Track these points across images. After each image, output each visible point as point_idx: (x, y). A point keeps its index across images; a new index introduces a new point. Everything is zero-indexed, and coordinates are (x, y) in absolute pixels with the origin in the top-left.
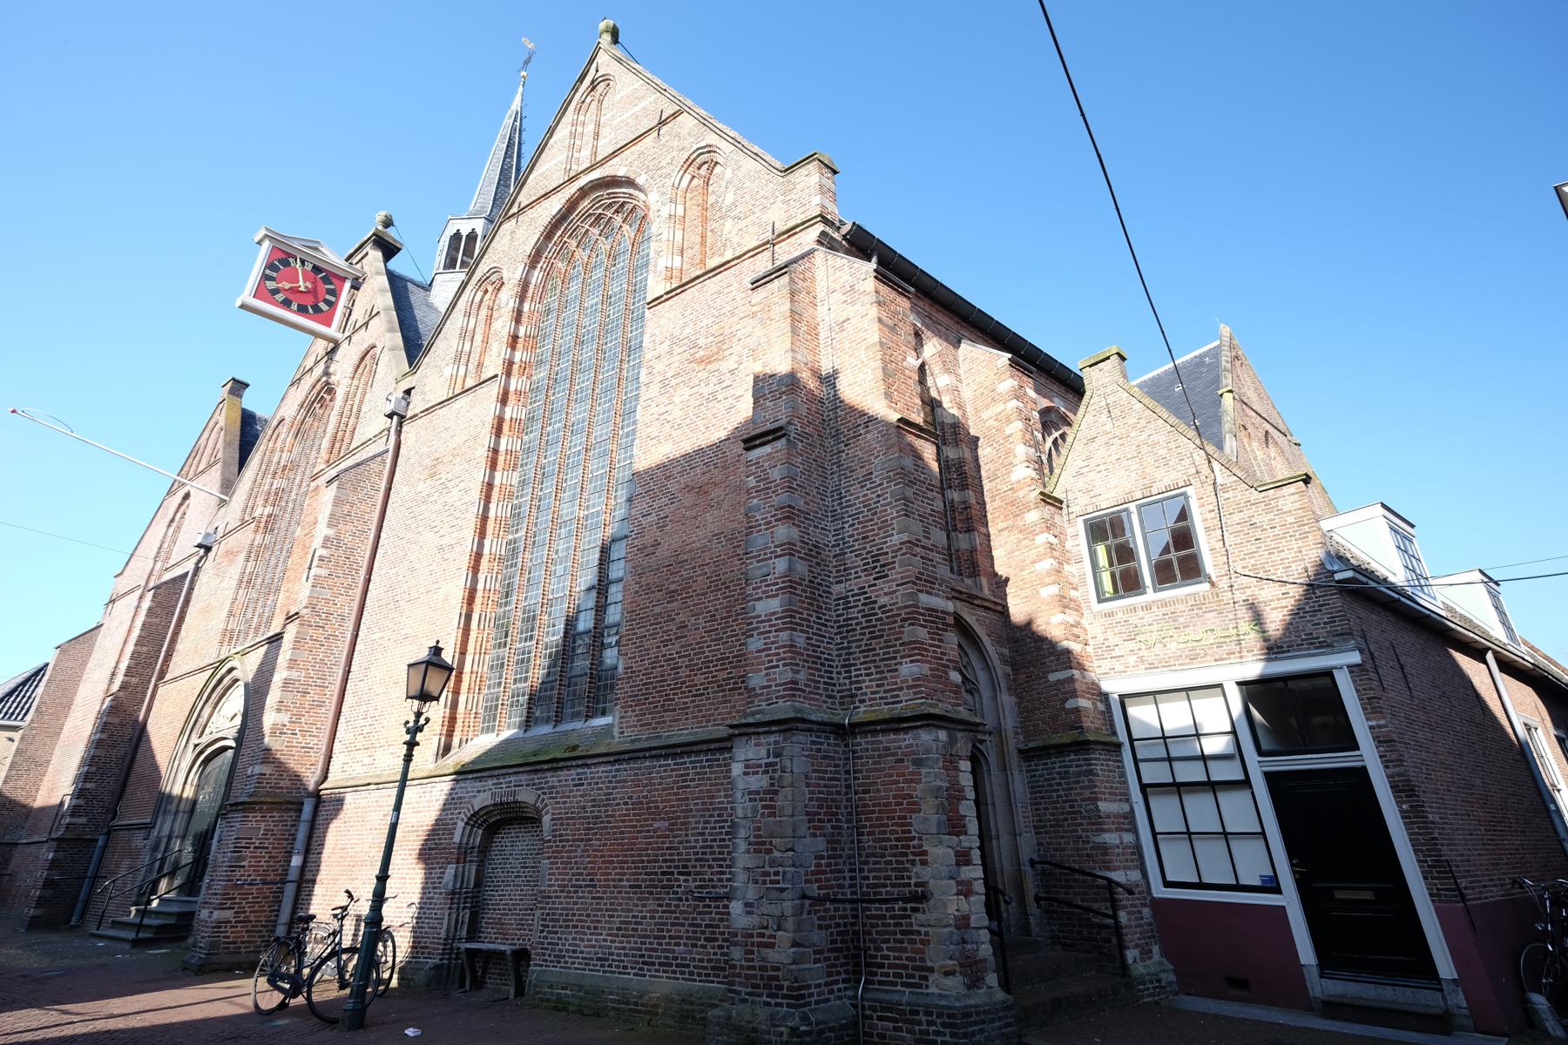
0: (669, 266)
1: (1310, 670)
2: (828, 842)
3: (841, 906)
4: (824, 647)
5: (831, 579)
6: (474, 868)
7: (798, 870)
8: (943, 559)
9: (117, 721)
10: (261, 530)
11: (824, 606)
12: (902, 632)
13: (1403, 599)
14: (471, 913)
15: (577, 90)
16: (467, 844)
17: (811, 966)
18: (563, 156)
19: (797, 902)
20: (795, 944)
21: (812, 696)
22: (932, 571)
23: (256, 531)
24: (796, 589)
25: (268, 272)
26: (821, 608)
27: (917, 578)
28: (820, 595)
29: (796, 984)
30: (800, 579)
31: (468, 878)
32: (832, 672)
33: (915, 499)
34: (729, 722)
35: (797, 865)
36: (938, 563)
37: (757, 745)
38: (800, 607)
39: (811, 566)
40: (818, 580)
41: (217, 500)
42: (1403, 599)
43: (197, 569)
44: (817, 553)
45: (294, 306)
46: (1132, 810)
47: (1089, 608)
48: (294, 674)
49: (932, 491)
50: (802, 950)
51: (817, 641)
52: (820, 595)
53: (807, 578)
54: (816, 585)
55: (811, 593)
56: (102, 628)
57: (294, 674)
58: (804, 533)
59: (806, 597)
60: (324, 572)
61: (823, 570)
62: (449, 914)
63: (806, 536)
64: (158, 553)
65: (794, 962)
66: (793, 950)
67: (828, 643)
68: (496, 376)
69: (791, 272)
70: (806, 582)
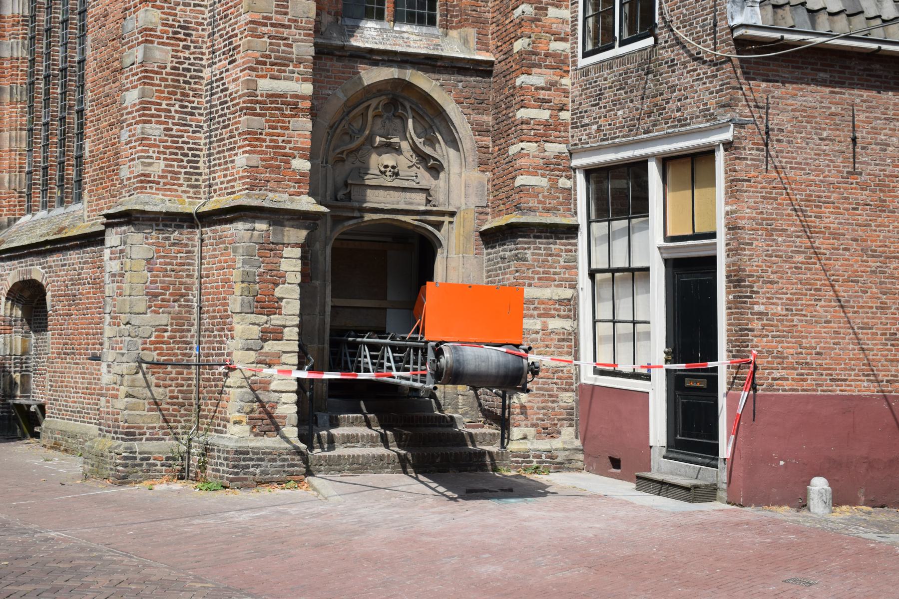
1: (676, 151)
2: (172, 318)
4: (188, 137)
5: (204, 63)
7: (135, 339)
8: (305, 35)
11: (191, 93)
12: (238, 122)
13: (885, 47)
14: (22, 376)
16: (11, 316)
17: (145, 413)
19: (132, 364)
20: (128, 395)
21: (168, 187)
22: (283, 52)
24: (152, 79)
26: (188, 96)
27: (258, 63)
29: (126, 424)
30: (159, 67)
31: (16, 345)
32: (197, 162)
34: (106, 212)
35: (132, 335)
36: (295, 41)
37: (116, 234)
38: (159, 97)
39: (177, 51)
40: (185, 66)
42: (885, 47)
44: (185, 34)
47: (574, 63)
50: (134, 400)
51: (178, 131)
52: (185, 82)
53: (169, 65)
54: (181, 72)
55: (173, 80)
58: (169, 14)
59: (166, 86)
61: (193, 53)
62: (3, 376)
63: (171, 18)
66: (126, 399)
67: (194, 132)
70: (168, 70)
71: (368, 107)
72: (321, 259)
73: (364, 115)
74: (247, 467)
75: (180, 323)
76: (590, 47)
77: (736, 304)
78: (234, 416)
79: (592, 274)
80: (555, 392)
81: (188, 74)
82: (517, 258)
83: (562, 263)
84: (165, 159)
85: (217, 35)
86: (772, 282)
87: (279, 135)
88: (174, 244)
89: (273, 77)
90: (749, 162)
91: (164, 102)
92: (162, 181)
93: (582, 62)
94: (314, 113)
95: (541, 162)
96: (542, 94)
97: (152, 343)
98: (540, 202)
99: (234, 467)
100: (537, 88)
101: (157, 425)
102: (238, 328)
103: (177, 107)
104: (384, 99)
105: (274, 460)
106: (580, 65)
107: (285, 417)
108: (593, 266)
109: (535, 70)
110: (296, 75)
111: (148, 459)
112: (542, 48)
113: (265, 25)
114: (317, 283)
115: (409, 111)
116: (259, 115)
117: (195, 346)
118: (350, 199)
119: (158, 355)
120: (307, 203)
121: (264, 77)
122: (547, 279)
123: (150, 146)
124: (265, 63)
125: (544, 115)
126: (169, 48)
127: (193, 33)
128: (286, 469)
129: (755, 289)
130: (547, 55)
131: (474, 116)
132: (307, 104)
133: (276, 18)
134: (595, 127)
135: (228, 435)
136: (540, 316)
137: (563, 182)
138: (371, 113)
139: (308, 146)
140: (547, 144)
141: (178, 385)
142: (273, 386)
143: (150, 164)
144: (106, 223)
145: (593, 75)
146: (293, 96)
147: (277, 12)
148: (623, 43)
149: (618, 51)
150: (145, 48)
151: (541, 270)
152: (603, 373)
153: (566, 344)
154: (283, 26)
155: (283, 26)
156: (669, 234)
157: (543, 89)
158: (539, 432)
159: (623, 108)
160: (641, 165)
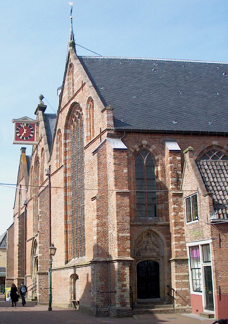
0: (87, 136)
3: (107, 293)
6: (73, 286)
9: (20, 251)
10: (34, 201)
11: (106, 236)
15: (67, 68)
18: (67, 92)
20: (96, 299)
23: (34, 201)
25: (17, 131)
28: (105, 234)
40: (105, 231)
41: (25, 191)
43: (26, 210)
45: (25, 139)
46: (189, 275)
48: (41, 245)
49: (127, 207)
52: (105, 234)
56: (15, 224)
57: (41, 245)
60: (41, 220)
64: (19, 203)
65: (96, 301)
68: (63, 165)
69: (98, 151)
71: (143, 236)
72: (134, 269)
73: (142, 237)
74: (120, 313)
75: (106, 283)
77: (216, 276)
78: (117, 302)
79: (191, 270)
80: (185, 296)
81: (106, 232)
83: (185, 267)
84: (102, 250)
85: (111, 224)
86: (223, 271)
87: (124, 245)
89: (122, 233)
90: (216, 247)
91: (101, 239)
92: (101, 254)
93: (187, 224)
94: (131, 239)
95: (179, 246)
96: (179, 231)
97: (101, 288)
98: (180, 254)
99: (118, 313)
100: (177, 230)
101: (102, 305)
102: (117, 284)
103: (104, 239)
104: (146, 234)
105: (125, 312)
107: (127, 303)
108: (192, 268)
109: (177, 226)
110: (127, 232)
111: (101, 312)
112: (178, 221)
113: (120, 223)
114: (134, 274)
115: (152, 236)
117: (109, 288)
118: (140, 256)
119: (188, 141)
120: (130, 258)
121: (120, 233)
122: (182, 271)
123: (99, 248)
124: (120, 230)
126: (101, 227)
127: (106, 224)
128: (128, 313)
129: (219, 273)
131: (166, 236)
132: (129, 238)
133: (122, 221)
135: (116, 307)
136: (181, 279)
137: (184, 250)
138: (143, 237)
139: (130, 246)
140: (180, 242)
141: (106, 296)
142: (125, 296)
143: (99, 251)
145: (189, 227)
146: (126, 237)
147: (122, 220)
149: (193, 222)
150: (97, 228)
151: (180, 269)
152: (195, 291)
153: (187, 285)
154: (123, 223)
155: (123, 223)
156: (204, 261)
157: (179, 230)
158: (182, 305)
160: (198, 246)
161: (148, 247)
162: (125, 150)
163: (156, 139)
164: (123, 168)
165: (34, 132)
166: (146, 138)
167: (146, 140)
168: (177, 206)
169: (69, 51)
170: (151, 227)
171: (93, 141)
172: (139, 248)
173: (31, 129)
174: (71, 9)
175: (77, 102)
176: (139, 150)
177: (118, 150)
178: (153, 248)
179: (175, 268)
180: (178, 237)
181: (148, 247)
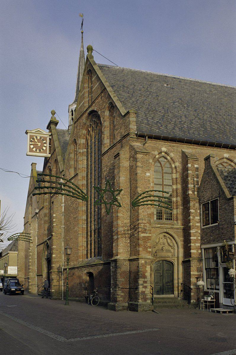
33: (143, 212)
45: (38, 151)
49: (148, 209)
76: (204, 224)
82: (105, 127)
88: (125, 265)
106: (202, 228)
116: (141, 240)
125: (195, 238)
130: (195, 226)
134: (206, 240)
144: (48, 239)
148: (211, 224)
149: (210, 225)
156: (223, 261)
159: (212, 237)
161: (164, 248)
162: (148, 154)
163: (174, 148)
164: (145, 171)
165: (47, 145)
166: (166, 145)
167: (166, 148)
168: (194, 211)
169: (87, 56)
170: (168, 229)
171: (112, 146)
172: (156, 249)
173: (44, 142)
174: (81, 23)
175: (95, 110)
176: (158, 157)
177: (141, 153)
178: (169, 249)
179: (78, 282)
180: (194, 239)
181: (164, 248)
